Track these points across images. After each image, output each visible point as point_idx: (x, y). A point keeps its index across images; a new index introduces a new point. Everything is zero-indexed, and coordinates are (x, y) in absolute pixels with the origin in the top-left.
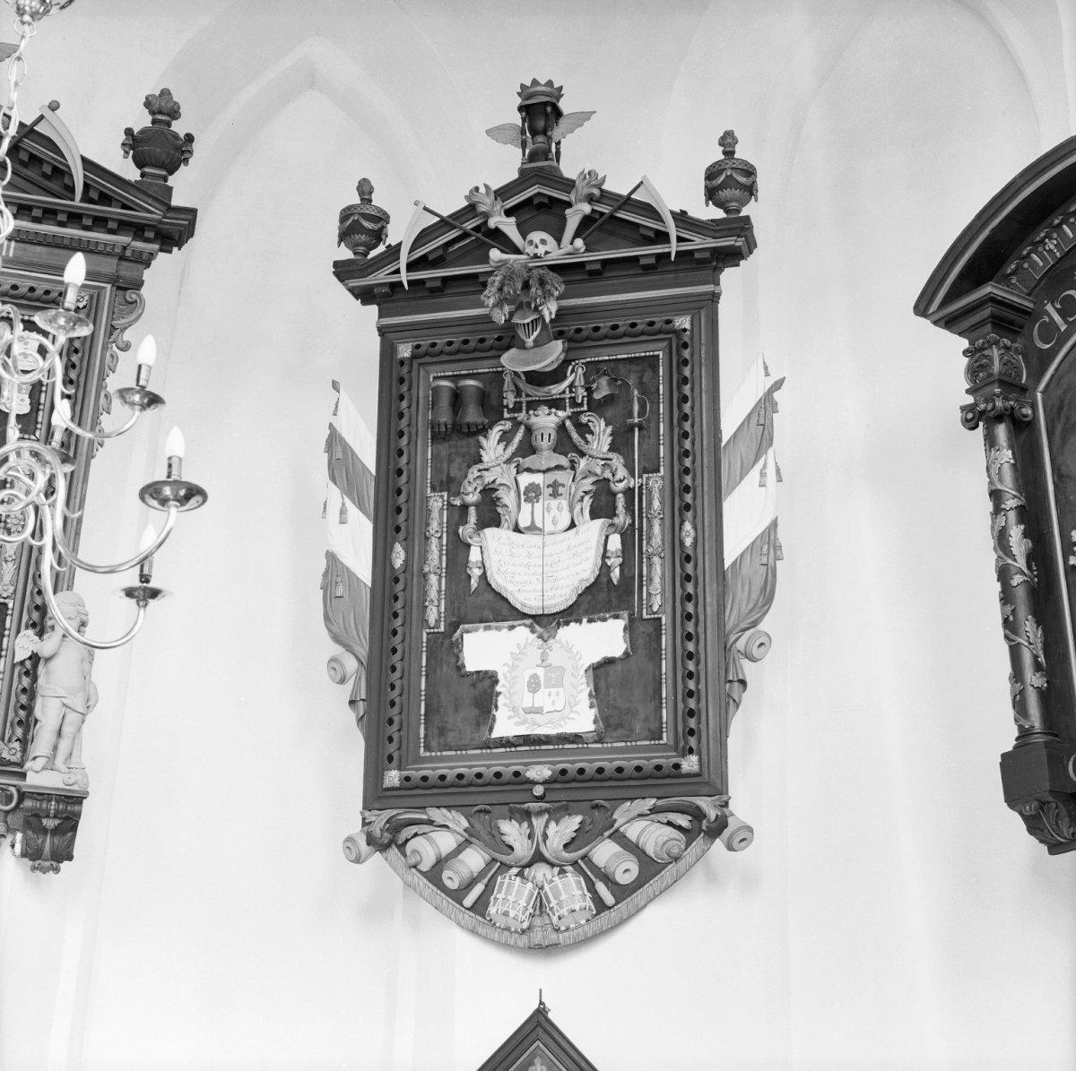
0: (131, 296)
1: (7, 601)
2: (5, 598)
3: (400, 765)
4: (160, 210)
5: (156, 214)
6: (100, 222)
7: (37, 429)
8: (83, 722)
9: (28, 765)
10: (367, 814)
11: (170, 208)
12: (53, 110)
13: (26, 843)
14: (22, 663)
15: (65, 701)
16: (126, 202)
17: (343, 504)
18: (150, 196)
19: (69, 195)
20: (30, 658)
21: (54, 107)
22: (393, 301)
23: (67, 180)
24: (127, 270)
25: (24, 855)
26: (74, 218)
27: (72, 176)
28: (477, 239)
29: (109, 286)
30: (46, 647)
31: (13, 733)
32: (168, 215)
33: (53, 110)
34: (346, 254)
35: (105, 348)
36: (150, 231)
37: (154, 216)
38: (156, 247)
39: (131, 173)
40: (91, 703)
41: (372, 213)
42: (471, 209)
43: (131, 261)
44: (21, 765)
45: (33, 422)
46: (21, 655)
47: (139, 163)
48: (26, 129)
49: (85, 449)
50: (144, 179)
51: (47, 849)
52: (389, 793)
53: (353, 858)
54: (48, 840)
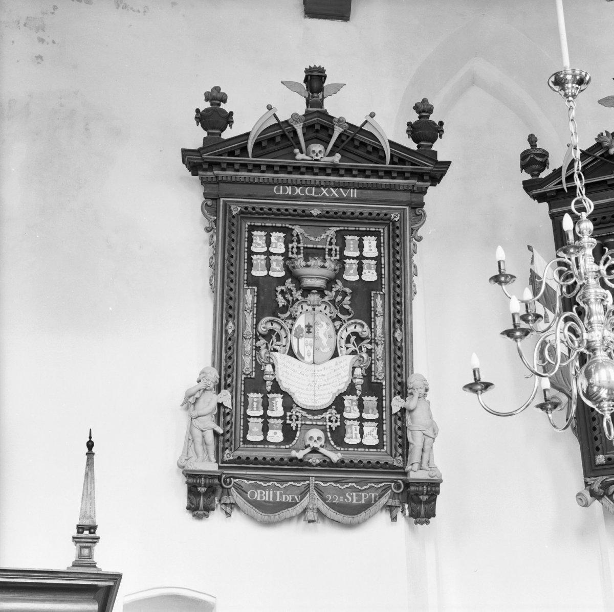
0: (418, 211)
1: (381, 381)
2: (380, 380)
3: (603, 452)
4: (431, 164)
5: (430, 166)
6: (401, 174)
7: (382, 288)
8: (434, 442)
9: (408, 468)
10: (588, 480)
11: (437, 162)
12: (372, 117)
13: (410, 508)
14: (396, 414)
15: (424, 432)
16: (413, 162)
17: (546, 312)
18: (427, 157)
19: (382, 161)
20: (400, 411)
21: (372, 115)
22: (557, 199)
23: (381, 154)
24: (415, 198)
25: (411, 515)
26: (388, 173)
27: (384, 151)
28: (601, 160)
29: (407, 208)
30: (411, 403)
31: (397, 451)
32: (436, 166)
33: (372, 117)
34: (528, 177)
35: (410, 241)
36: (426, 176)
37: (429, 168)
38: (429, 184)
39: (414, 146)
40: (436, 432)
41: (541, 153)
42: (599, 145)
43: (416, 193)
44: (403, 468)
45: (379, 285)
46: (395, 410)
47: (416, 140)
48: (358, 129)
49: (409, 296)
50: (421, 148)
51: (423, 512)
52: (599, 468)
53: (584, 504)
54: (202, 499)
